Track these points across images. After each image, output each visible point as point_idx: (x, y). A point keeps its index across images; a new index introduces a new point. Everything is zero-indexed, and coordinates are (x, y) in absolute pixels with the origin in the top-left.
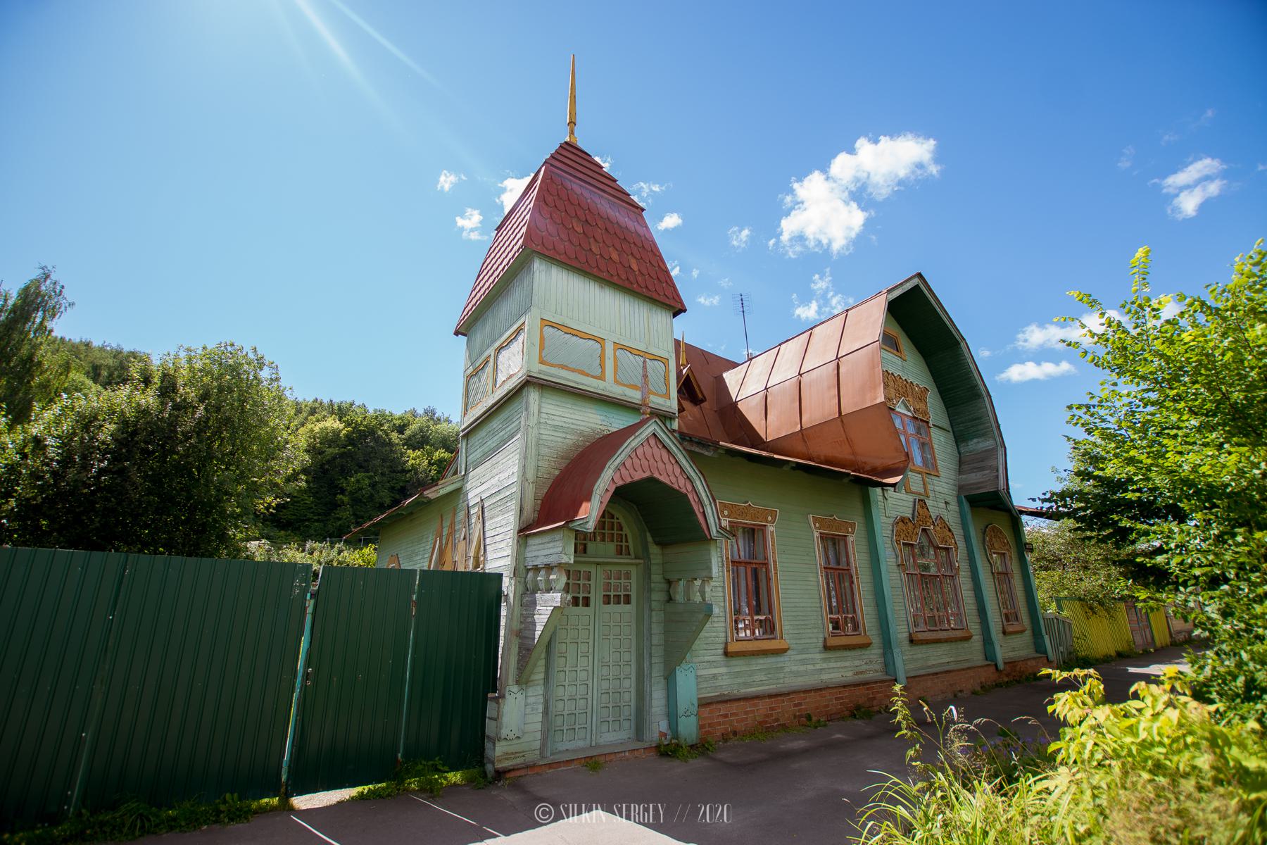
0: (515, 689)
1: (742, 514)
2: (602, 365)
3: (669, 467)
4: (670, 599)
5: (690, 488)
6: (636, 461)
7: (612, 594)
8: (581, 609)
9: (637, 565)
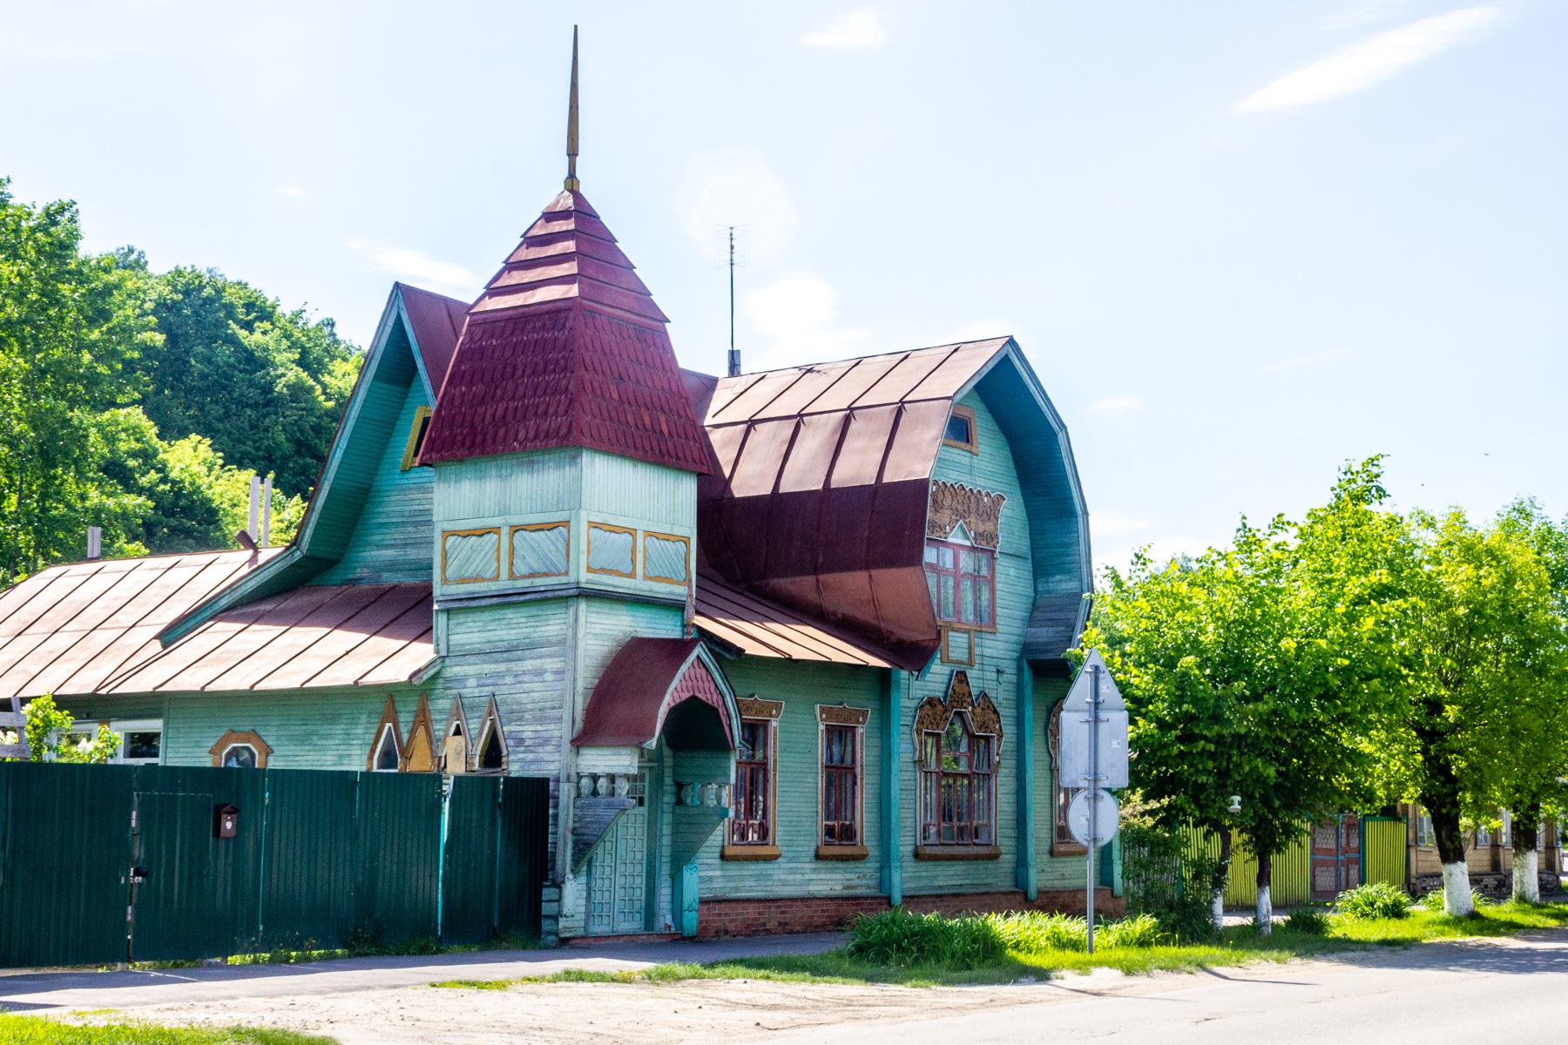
2: (633, 561)
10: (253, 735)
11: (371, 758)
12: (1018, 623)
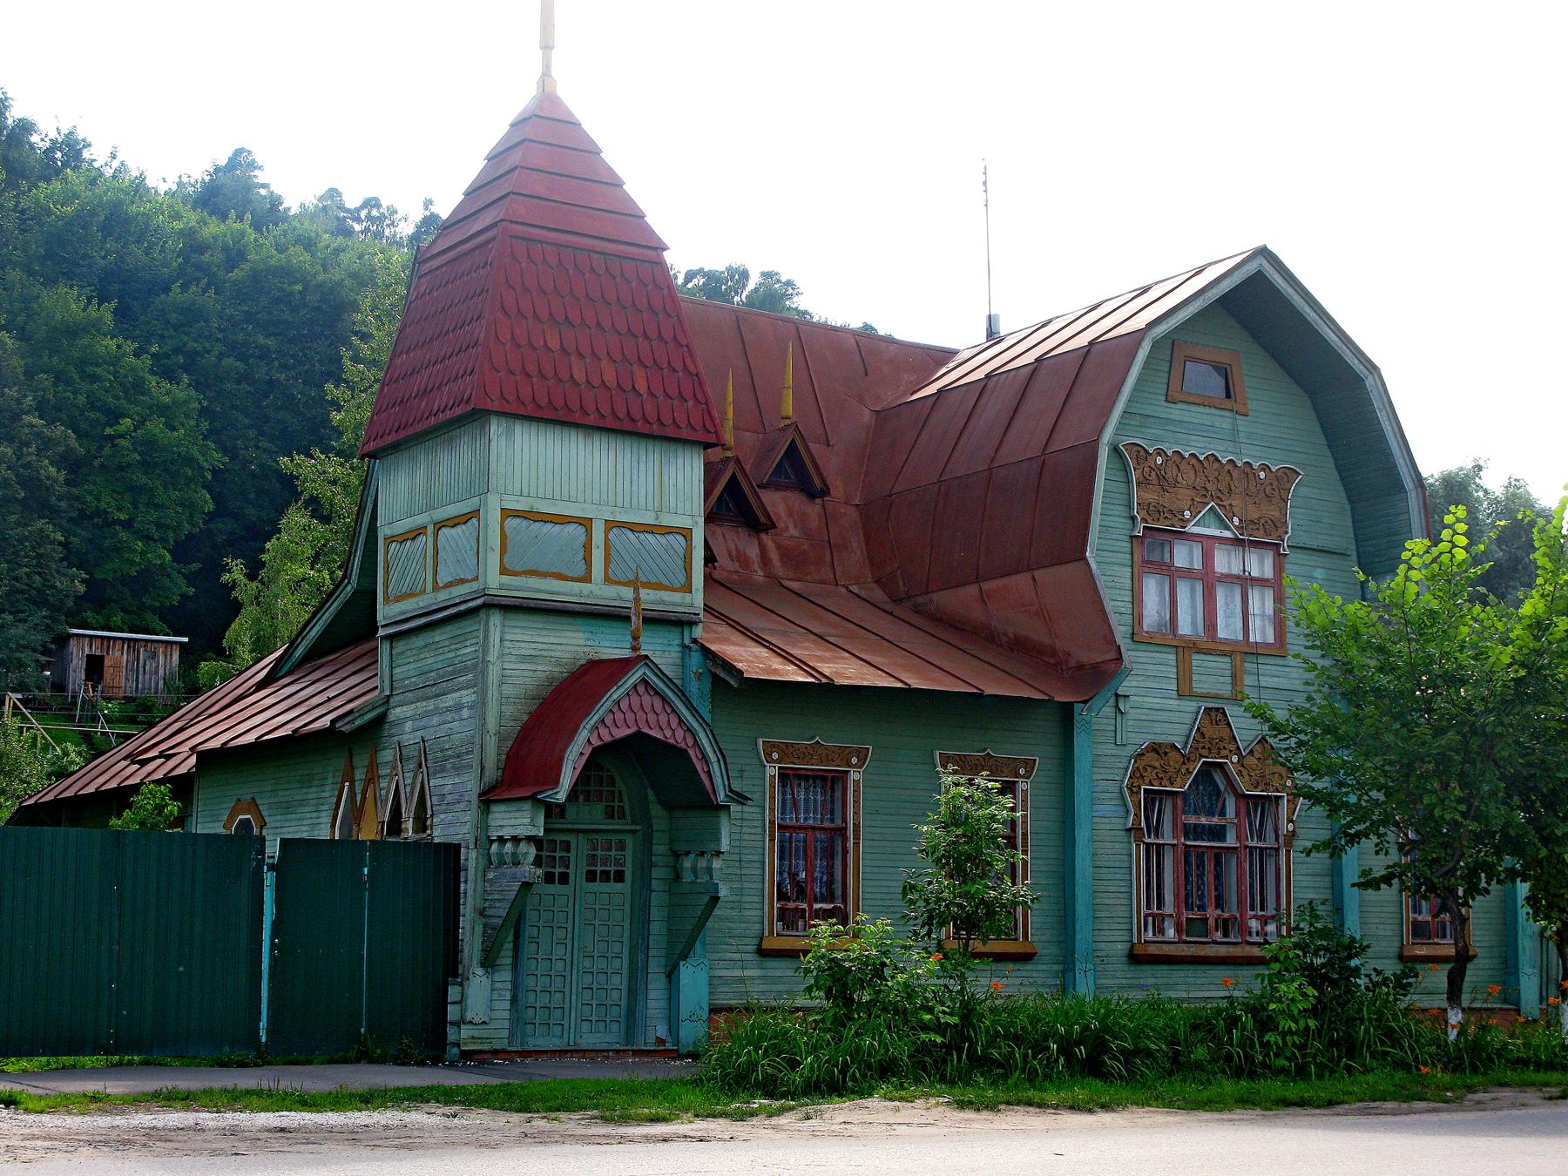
0: (480, 971)
1: (805, 755)
2: (588, 560)
3: (663, 718)
4: (677, 876)
5: (690, 742)
6: (619, 716)
7: (599, 869)
8: (556, 888)
9: (634, 832)
10: (253, 806)
11: (333, 826)
12: (589, 441)
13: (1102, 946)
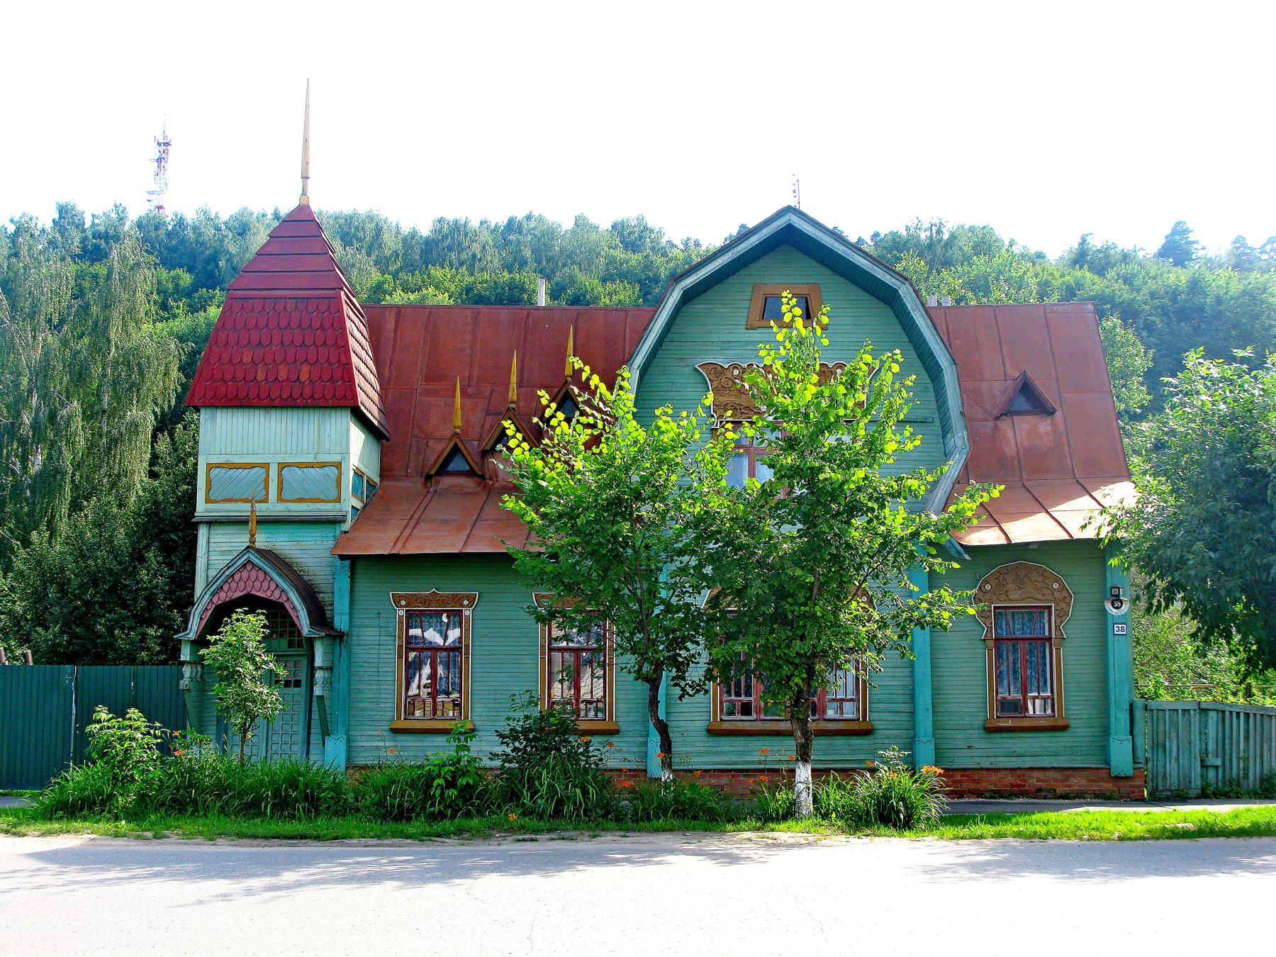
2: (267, 488)
13: (682, 724)
